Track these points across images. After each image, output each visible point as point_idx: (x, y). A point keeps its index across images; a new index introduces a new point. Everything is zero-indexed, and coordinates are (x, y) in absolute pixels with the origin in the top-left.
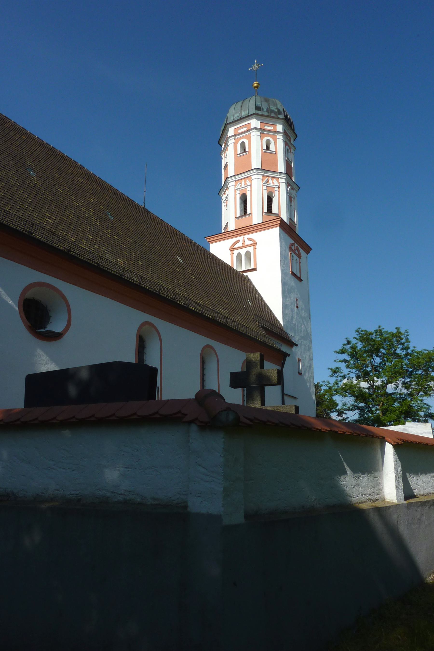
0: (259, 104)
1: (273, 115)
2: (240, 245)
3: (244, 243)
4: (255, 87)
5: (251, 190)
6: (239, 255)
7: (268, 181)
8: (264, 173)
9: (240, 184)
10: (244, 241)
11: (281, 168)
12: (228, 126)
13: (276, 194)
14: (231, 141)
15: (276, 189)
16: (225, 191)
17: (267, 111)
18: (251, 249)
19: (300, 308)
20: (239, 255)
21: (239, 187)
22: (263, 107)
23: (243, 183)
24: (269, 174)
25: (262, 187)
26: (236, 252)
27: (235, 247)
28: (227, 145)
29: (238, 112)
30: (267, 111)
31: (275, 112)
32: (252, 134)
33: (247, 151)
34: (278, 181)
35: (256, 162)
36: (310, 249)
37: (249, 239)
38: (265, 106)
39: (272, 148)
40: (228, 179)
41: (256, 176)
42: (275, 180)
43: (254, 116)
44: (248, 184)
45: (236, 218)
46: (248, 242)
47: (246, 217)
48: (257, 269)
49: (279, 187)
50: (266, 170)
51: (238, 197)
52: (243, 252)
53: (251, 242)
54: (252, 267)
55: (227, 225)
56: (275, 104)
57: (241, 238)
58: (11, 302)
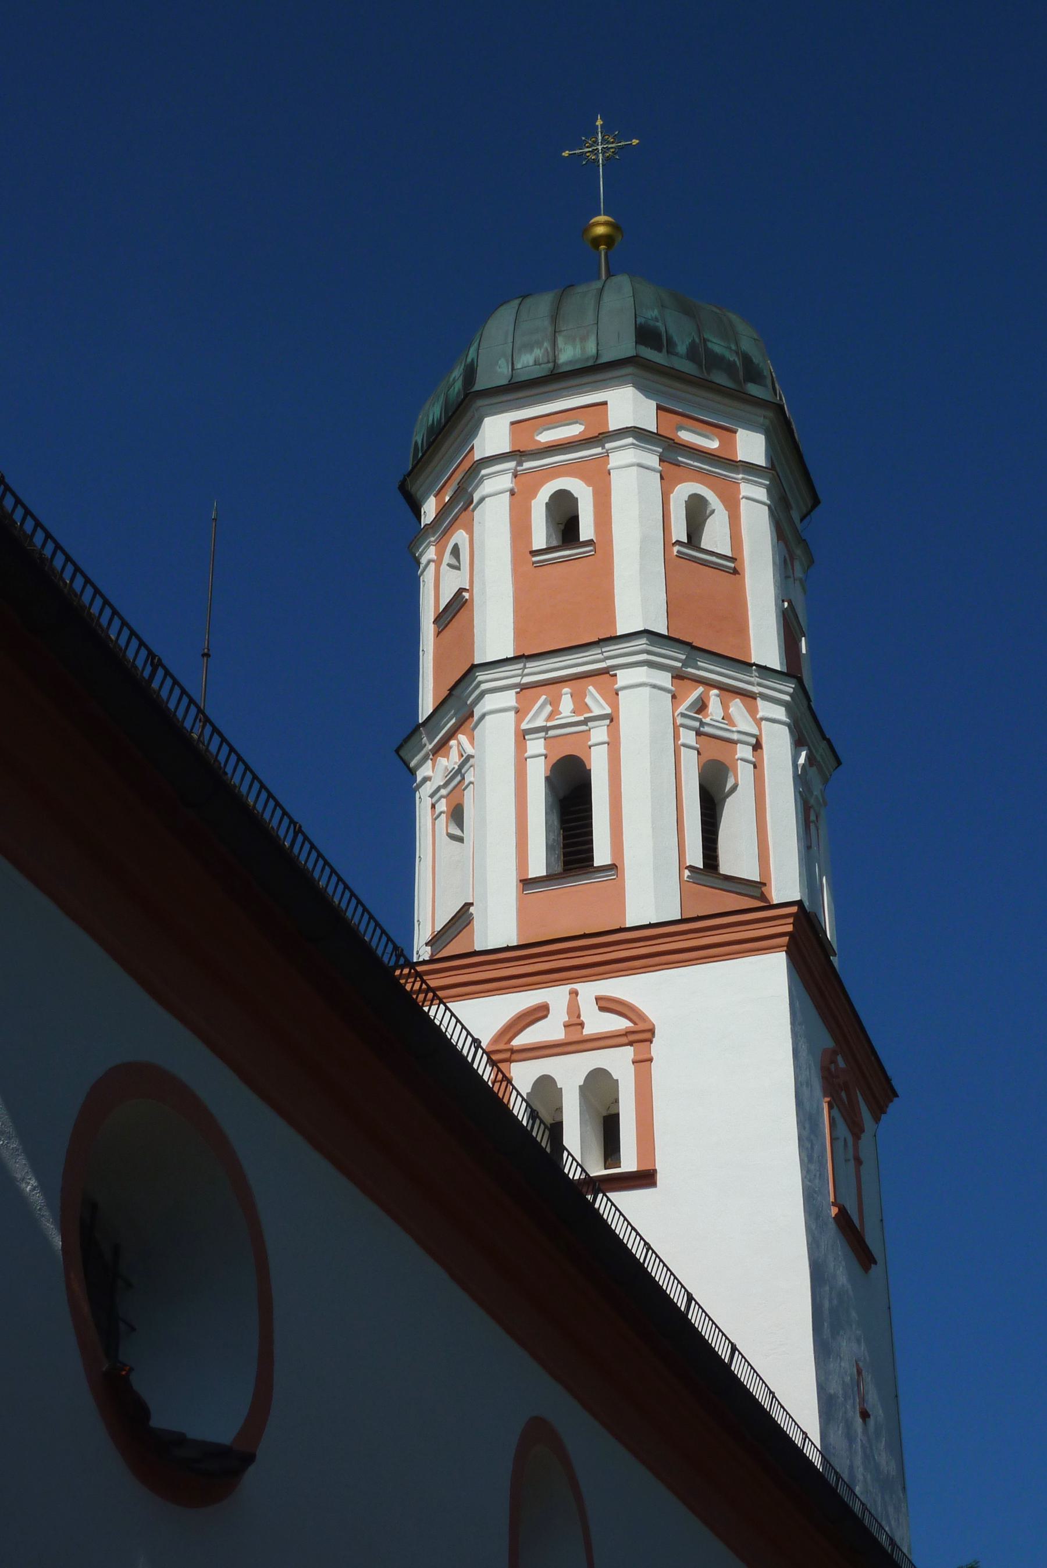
0: (651, 314)
1: (721, 378)
3: (575, 1023)
4: (597, 241)
5: (614, 745)
7: (701, 706)
8: (685, 663)
9: (549, 709)
10: (574, 1009)
11: (765, 646)
12: (480, 403)
13: (744, 774)
14: (496, 485)
15: (744, 752)
16: (451, 735)
17: (692, 354)
18: (618, 1062)
19: (871, 1422)
21: (540, 722)
22: (673, 331)
23: (566, 705)
24: (707, 670)
25: (676, 736)
27: (521, 1040)
28: (462, 504)
29: (539, 344)
30: (692, 354)
31: (729, 368)
32: (616, 460)
33: (590, 543)
34: (753, 711)
35: (638, 600)
37: (606, 1005)
38: (681, 332)
39: (716, 537)
40: (481, 676)
41: (641, 674)
42: (737, 706)
43: (629, 370)
44: (597, 712)
45: (527, 883)
46: (598, 1022)
47: (580, 888)
48: (660, 1178)
49: (757, 746)
50: (694, 650)
51: (537, 773)
53: (618, 1023)
54: (629, 1163)
55: (463, 918)
56: (729, 333)
57: (556, 996)
58: (29, 1185)
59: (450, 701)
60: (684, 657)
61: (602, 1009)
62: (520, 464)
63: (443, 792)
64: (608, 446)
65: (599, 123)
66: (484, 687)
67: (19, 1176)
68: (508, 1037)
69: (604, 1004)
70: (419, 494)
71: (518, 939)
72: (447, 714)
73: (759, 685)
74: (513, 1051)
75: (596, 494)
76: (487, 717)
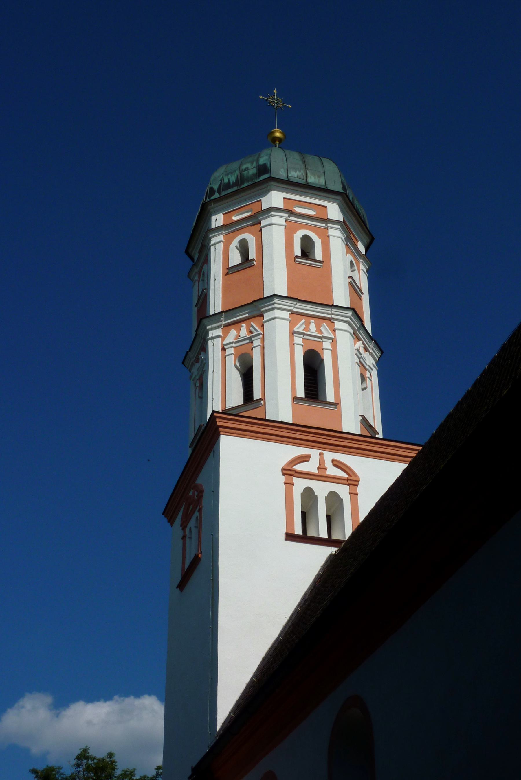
2: (311, 467)
3: (322, 467)
6: (309, 496)
12: (273, 183)
18: (343, 491)
20: (309, 496)
26: (300, 484)
36: (286, 539)
37: (336, 464)
40: (276, 301)
41: (346, 326)
43: (339, 198)
45: (296, 399)
46: (333, 471)
52: (321, 490)
57: (315, 453)
59: (251, 305)
61: (334, 465)
62: (289, 217)
63: (234, 345)
64: (329, 225)
66: (276, 305)
68: (293, 465)
69: (334, 463)
70: (212, 210)
72: (246, 310)
73: (372, 349)
74: (296, 472)
75: (323, 243)
76: (276, 320)
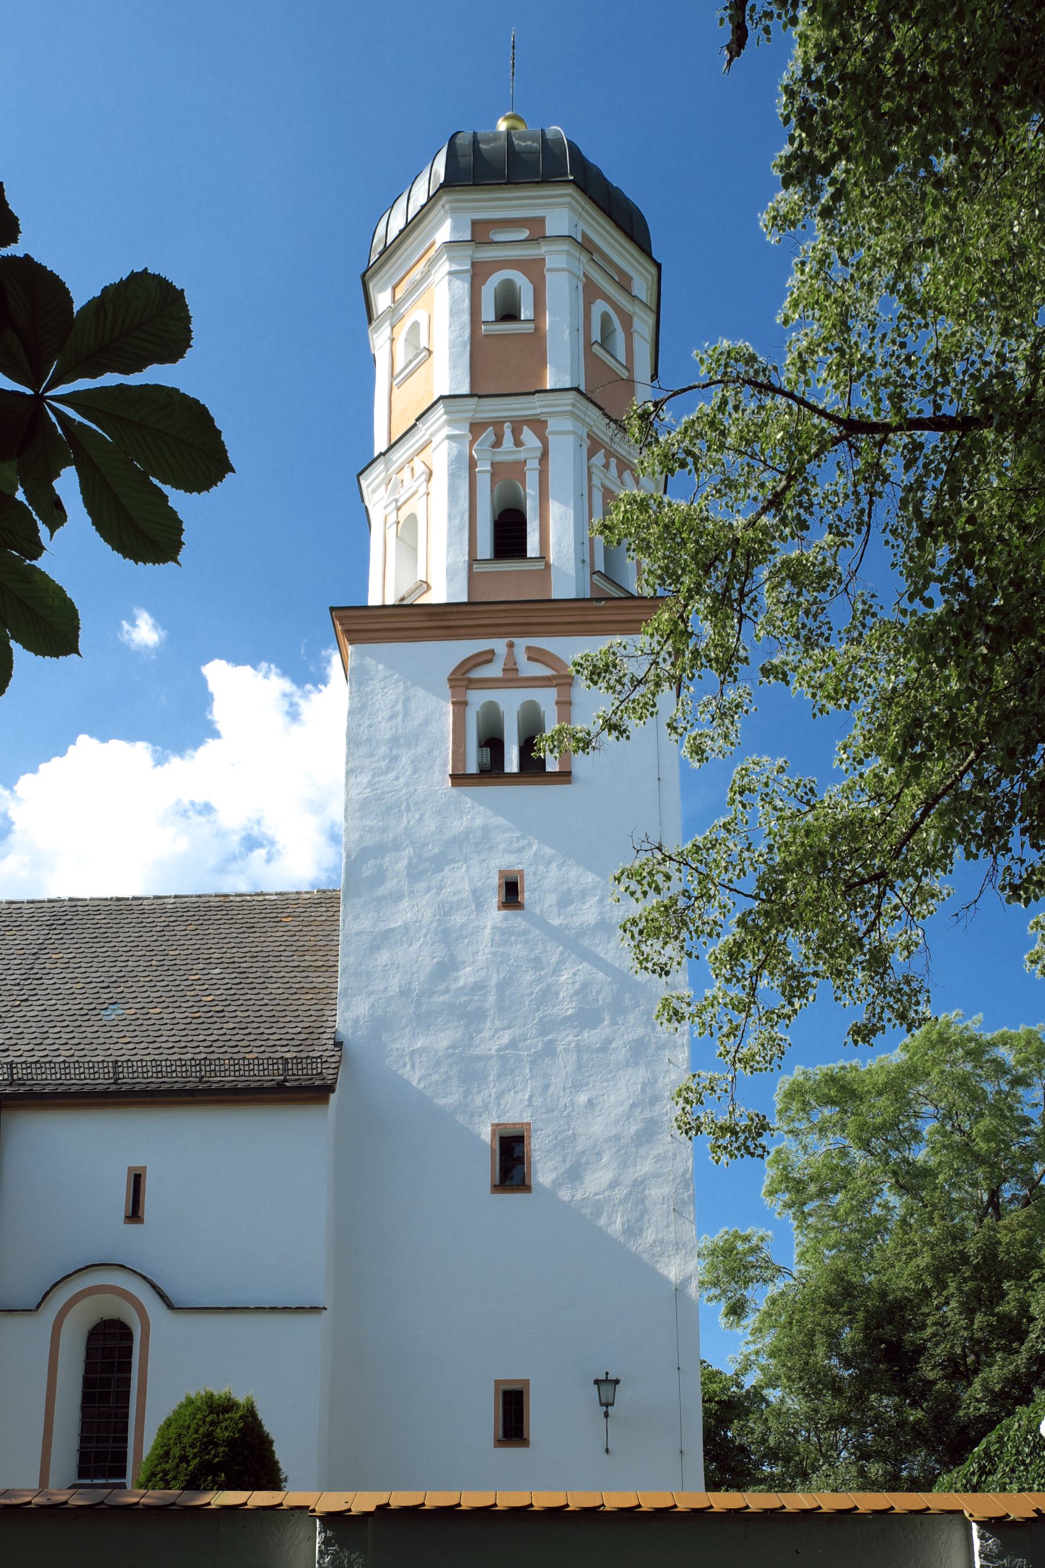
10: (511, 655)
18: (546, 699)
37: (535, 655)
57: (499, 645)
60: (382, 467)
65: (20, 495)
67: (451, 1099)
71: (448, 597)
